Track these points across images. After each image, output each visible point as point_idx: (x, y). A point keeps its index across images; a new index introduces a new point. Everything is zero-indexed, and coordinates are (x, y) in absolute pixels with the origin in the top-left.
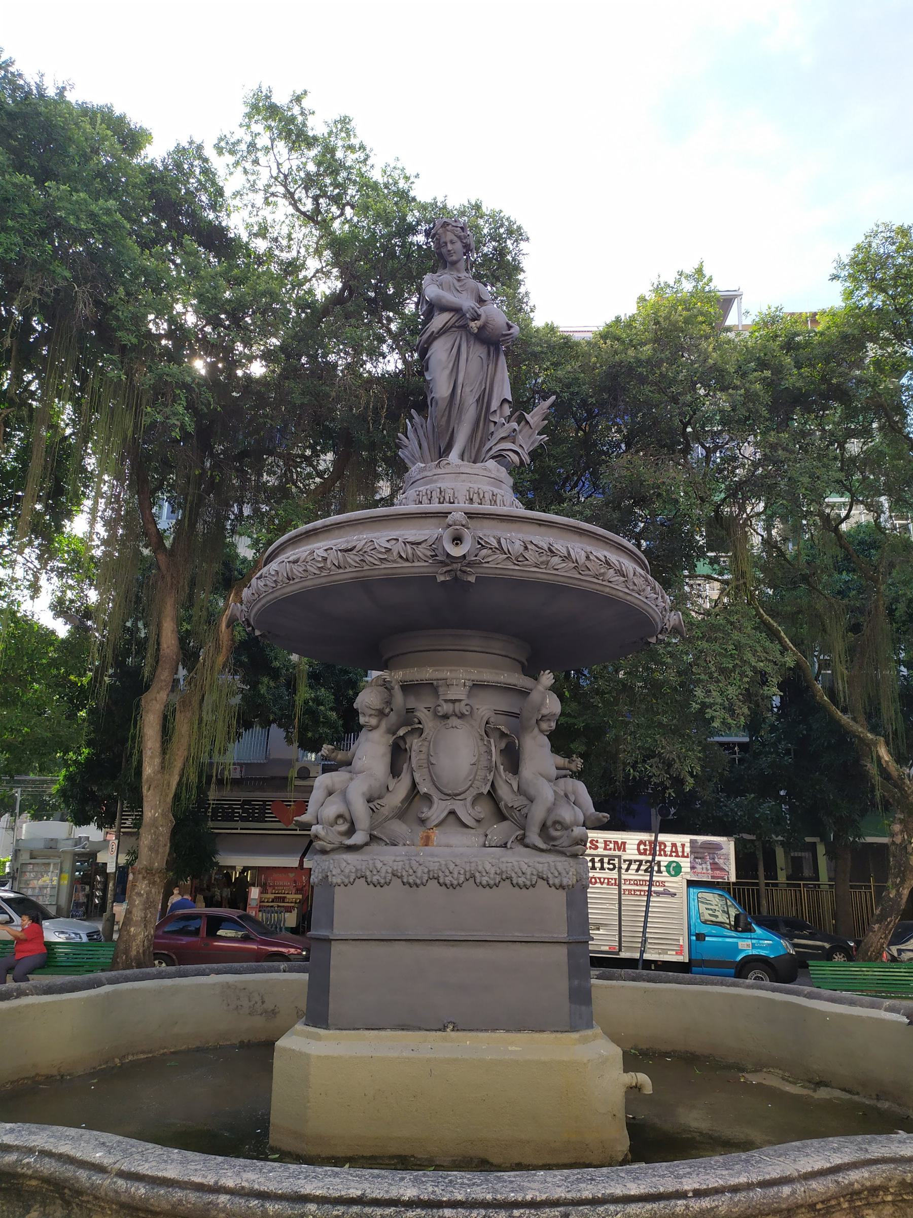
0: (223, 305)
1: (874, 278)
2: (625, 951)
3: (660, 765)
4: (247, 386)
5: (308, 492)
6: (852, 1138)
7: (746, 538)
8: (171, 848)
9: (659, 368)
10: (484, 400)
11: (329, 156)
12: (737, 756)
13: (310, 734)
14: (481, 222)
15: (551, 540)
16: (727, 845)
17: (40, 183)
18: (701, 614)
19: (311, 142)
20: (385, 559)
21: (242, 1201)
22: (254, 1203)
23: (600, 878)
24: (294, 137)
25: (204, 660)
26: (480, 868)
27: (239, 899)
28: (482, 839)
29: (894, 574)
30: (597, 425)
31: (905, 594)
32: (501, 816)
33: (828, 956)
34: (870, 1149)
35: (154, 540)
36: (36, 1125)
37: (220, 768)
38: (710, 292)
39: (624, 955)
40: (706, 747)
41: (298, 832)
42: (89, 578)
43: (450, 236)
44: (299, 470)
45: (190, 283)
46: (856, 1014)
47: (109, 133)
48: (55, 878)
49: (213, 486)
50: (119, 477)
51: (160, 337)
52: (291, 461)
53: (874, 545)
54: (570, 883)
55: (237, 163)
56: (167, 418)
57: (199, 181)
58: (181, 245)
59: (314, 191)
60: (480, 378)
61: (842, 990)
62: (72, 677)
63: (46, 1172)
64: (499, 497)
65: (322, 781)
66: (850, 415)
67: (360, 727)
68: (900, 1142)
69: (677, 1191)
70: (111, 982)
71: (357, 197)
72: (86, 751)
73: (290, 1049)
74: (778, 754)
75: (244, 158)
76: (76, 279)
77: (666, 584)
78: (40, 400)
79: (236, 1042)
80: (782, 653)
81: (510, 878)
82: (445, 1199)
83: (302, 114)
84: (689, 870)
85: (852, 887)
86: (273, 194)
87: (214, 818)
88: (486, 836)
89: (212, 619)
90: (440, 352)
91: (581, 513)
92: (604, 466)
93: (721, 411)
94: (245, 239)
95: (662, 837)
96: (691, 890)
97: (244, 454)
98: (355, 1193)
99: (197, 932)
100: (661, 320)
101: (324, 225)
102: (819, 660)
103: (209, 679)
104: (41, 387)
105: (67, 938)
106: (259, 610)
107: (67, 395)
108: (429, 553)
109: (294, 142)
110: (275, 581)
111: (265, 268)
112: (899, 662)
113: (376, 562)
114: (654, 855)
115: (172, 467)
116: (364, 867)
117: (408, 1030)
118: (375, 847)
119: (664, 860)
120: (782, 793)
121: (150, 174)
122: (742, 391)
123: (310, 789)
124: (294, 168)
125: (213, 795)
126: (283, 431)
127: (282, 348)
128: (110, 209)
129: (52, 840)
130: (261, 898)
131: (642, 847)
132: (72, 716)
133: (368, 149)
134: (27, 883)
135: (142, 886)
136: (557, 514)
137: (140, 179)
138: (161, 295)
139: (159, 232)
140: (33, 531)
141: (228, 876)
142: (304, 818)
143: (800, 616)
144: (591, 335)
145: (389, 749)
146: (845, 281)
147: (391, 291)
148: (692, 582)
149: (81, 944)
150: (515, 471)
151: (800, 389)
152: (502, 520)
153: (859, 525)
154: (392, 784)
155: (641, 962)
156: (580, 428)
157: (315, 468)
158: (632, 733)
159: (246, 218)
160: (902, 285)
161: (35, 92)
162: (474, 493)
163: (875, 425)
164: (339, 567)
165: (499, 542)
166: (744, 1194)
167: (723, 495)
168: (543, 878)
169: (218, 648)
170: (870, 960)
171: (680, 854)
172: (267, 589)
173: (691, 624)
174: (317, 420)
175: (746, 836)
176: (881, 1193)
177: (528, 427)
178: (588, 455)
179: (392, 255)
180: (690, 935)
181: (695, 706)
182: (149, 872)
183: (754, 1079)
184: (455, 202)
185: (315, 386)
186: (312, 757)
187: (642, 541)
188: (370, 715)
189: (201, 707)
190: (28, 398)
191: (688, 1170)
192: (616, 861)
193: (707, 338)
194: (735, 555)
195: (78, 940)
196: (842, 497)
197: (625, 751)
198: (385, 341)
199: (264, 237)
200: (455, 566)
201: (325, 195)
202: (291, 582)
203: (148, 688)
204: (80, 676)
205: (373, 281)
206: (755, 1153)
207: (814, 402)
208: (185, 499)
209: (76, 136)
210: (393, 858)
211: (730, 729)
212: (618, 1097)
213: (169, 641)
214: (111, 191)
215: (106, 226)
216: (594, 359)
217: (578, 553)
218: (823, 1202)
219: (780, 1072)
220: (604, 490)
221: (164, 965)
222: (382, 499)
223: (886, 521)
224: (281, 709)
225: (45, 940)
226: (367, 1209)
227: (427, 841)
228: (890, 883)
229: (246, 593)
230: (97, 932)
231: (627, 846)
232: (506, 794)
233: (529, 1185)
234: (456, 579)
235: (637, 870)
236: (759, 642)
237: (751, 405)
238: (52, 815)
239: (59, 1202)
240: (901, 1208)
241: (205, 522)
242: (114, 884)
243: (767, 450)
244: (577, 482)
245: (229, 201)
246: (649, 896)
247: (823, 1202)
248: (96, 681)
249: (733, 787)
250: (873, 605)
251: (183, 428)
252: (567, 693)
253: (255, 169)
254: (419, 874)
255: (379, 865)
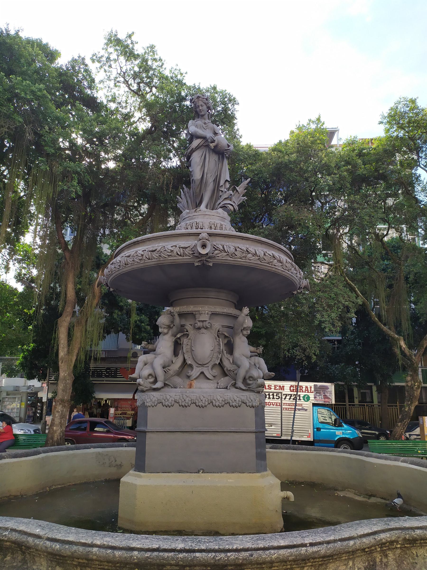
0: (95, 134)
1: (399, 123)
2: (284, 436)
3: (300, 350)
4: (107, 173)
5: (136, 223)
6: (382, 519)
7: (340, 244)
8: (73, 390)
9: (300, 165)
10: (217, 181)
11: (145, 63)
12: (336, 346)
13: (137, 337)
14: (216, 95)
15: (248, 246)
16: (331, 387)
17: (7, 75)
18: (319, 280)
19: (136, 57)
20: (170, 255)
21: (104, 550)
22: (109, 551)
23: (272, 403)
24: (128, 54)
25: (88, 302)
26: (215, 398)
27: (105, 414)
28: (216, 385)
30: (271, 192)
31: (413, 271)
32: (225, 374)
33: (377, 438)
34: (390, 524)
35: (63, 246)
36: (9, 517)
37: (96, 352)
38: (323, 129)
39: (283, 438)
40: (321, 342)
41: (132, 382)
42: (33, 264)
43: (200, 103)
44: (131, 212)
45: (79, 124)
46: (387, 464)
47: (40, 52)
48: (18, 405)
49: (91, 220)
50: (46, 216)
51: (65, 149)
52: (128, 208)
53: (399, 248)
54: (257, 405)
55: (101, 67)
56: (69, 188)
57: (83, 75)
58: (75, 106)
59: (138, 80)
60: (215, 170)
61: (383, 453)
62: (25, 310)
63: (14, 539)
64: (224, 226)
65: (142, 358)
66: (388, 187)
67: (160, 333)
68: (404, 520)
69: (302, 543)
70: (44, 452)
71: (158, 83)
72: (32, 345)
73: (127, 482)
74: (355, 345)
75: (104, 64)
76: (25, 122)
77: (302, 266)
78: (8, 179)
79: (103, 479)
80: (356, 298)
81: (229, 403)
82: (196, 549)
83: (132, 43)
84: (313, 398)
85: (389, 406)
86: (118, 82)
87: (93, 376)
88: (218, 383)
89: (91, 283)
90: (196, 157)
91: (263, 233)
92: (274, 211)
93: (329, 185)
94: (105, 102)
95: (301, 384)
96: (314, 408)
97: (105, 205)
98: (155, 546)
99: (85, 429)
100: (300, 142)
101: (143, 96)
102: (374, 301)
103: (90, 311)
104: (9, 173)
105: (24, 432)
106: (112, 278)
107: (21, 177)
108: (191, 252)
109: (128, 57)
110: (119, 265)
111: (115, 117)
112: (411, 302)
113: (166, 257)
114: (297, 392)
116: (178, 398)
117: (182, 473)
118: (166, 389)
119: (302, 394)
120: (357, 363)
121: (60, 72)
122: (338, 176)
123: (136, 362)
124: (128, 69)
125: (92, 365)
126: (124, 194)
127: (123, 155)
128: (41, 89)
129: (17, 386)
130: (115, 413)
131: (292, 388)
132: (25, 328)
133: (163, 60)
134: (5, 406)
135: (59, 408)
136: (252, 234)
137: (55, 74)
138: (65, 129)
139: (65, 99)
140: (6, 241)
141: (100, 403)
142: (134, 376)
143: (365, 281)
144: (267, 149)
145: (173, 343)
146: (386, 124)
147: (174, 128)
148: (315, 265)
149: (31, 435)
150: (232, 214)
151: (365, 175)
152: (225, 237)
153: (393, 238)
154: (174, 360)
155: (291, 441)
156: (263, 193)
157: (139, 212)
158: (287, 336)
159: (106, 93)
160: (412, 126)
161: (5, 32)
162: (212, 224)
163: (400, 192)
164: (149, 259)
165: (223, 247)
166: (332, 544)
167: (329, 225)
168: (244, 403)
169: (94, 296)
170: (396, 439)
171: (309, 391)
172: (115, 269)
173: (314, 284)
174: (140, 189)
175: (340, 383)
176: (395, 544)
177: (237, 193)
178: (266, 205)
180: (314, 428)
181: (317, 322)
182: (62, 401)
183: (342, 494)
184: (204, 85)
185: (139, 173)
186: (139, 347)
187: (292, 246)
188: (164, 328)
189: (86, 324)
190: (3, 179)
191: (308, 534)
192: (280, 395)
193: (322, 150)
194: (335, 252)
195: (29, 433)
196: (384, 225)
197: (284, 344)
198: (172, 152)
199: (114, 102)
200: (203, 258)
201: (143, 82)
202: (127, 266)
203: (61, 315)
204: (29, 310)
205: (166, 123)
206: (338, 527)
207: (372, 181)
208: (78, 226)
210: (175, 394)
211: (332, 333)
212: (278, 503)
213: (71, 294)
214: (41, 80)
215: (39, 97)
216: (269, 161)
217: (260, 252)
218: (368, 548)
219: (354, 491)
220: (274, 222)
221: (70, 444)
222: (171, 226)
223: (405, 236)
224: (124, 325)
225: (14, 433)
226: (161, 553)
227: (190, 386)
228: (405, 404)
229: (106, 271)
230: (38, 429)
231: (285, 388)
232: (227, 364)
233: (235, 542)
234: (203, 264)
235: (290, 399)
236: (346, 293)
237: (342, 182)
238: (17, 375)
239: (20, 552)
240: (404, 551)
241: (88, 237)
242: (46, 407)
243: (350, 204)
244: (262, 218)
245: (98, 85)
246: (295, 410)
247: (368, 548)
248: (37, 312)
249: (334, 360)
250: (398, 276)
251: (76, 193)
252: (257, 317)
253: (110, 70)
254: (187, 401)
255: (168, 397)
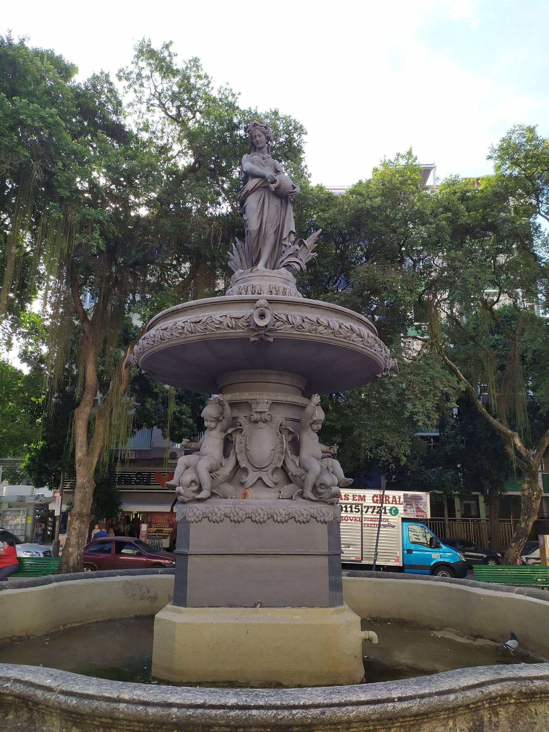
0: (122, 172)
1: (513, 158)
2: (365, 560)
3: (386, 450)
4: (138, 222)
5: (175, 286)
6: (491, 666)
7: (437, 314)
8: (93, 500)
9: (385, 211)
10: (279, 232)
11: (186, 81)
12: (432, 444)
13: (177, 433)
14: (278, 122)
15: (319, 316)
16: (426, 497)
17: (10, 97)
18: (410, 359)
19: (175, 73)
20: (219, 328)
21: (133, 707)
22: (140, 708)
23: (350, 517)
24: (165, 70)
25: (113, 388)
26: (276, 512)
27: (135, 531)
28: (278, 494)
29: (525, 336)
30: (348, 246)
31: (531, 348)
32: (289, 481)
33: (485, 562)
34: (502, 673)
35: (82, 315)
36: (11, 665)
37: (123, 453)
38: (416, 165)
39: (364, 562)
40: (413, 439)
41: (170, 491)
42: (43, 339)
43: (258, 132)
44: (169, 273)
45: (102, 159)
46: (498, 595)
47: (51, 66)
48: (24, 519)
49: (117, 283)
50: (60, 277)
51: (84, 192)
52: (164, 268)
53: (513, 318)
54: (330, 520)
55: (130, 86)
56: (89, 241)
57: (107, 97)
58: (96, 136)
59: (177, 103)
60: (277, 218)
61: (492, 582)
62: (33, 399)
63: (18, 692)
64: (288, 290)
65: (182, 460)
66: (499, 240)
67: (206, 428)
68: (519, 668)
69: (388, 698)
70: (57, 580)
71: (203, 107)
72: (41, 443)
73: (164, 619)
74: (456, 443)
75: (134, 83)
76: (32, 156)
77: (388, 342)
78: (11, 230)
79: (132, 615)
80: (458, 383)
81: (294, 517)
82: (252, 704)
83: (170, 55)
84: (403, 512)
85: (500, 521)
86: (152, 105)
87: (119, 483)
88: (280, 492)
89: (117, 363)
90: (252, 202)
91: (338, 299)
92: (353, 271)
93: (422, 238)
94: (135, 131)
95: (387, 493)
96: (404, 523)
97: (135, 264)
98: (200, 701)
99: (109, 551)
100: (386, 183)
101: (183, 124)
102: (480, 386)
103: (115, 399)
104: (11, 222)
105: (31, 555)
106: (144, 358)
107: (27, 227)
108: (245, 324)
109: (165, 73)
110: (153, 341)
111: (147, 150)
112: (528, 388)
113: (214, 330)
114: (382, 503)
115: (92, 271)
116: (229, 511)
117: (234, 607)
118: (213, 500)
119: (388, 506)
120: (459, 466)
121: (77, 92)
122: (434, 226)
123: (175, 465)
124: (165, 89)
125: (118, 469)
126: (159, 249)
127: (158, 199)
129: (22, 496)
130: (148, 530)
131: (375, 498)
132: (33, 422)
133: (210, 77)
134: (7, 522)
135: (76, 524)
136: (324, 300)
137: (71, 95)
138: (84, 166)
139: (83, 127)
140: (8, 310)
141: (128, 518)
142: (172, 482)
143: (469, 360)
144: (344, 191)
145: (223, 441)
146: (496, 160)
147: (224, 164)
148: (405, 340)
149: (40, 559)
150: (299, 275)
151: (469, 225)
152: (289, 304)
153: (505, 306)
154: (224, 462)
155: (374, 567)
156: (338, 248)
157: (179, 272)
158: (369, 431)
159: (136, 119)
160: (529, 162)
161: (6, 41)
162: (273, 288)
163: (514, 246)
164: (192, 333)
165: (287, 318)
166: (427, 699)
167: (423, 288)
168: (313, 517)
169: (121, 381)
170: (510, 564)
171: (398, 502)
172: (148, 346)
173: (404, 365)
174: (180, 243)
175: (437, 492)
176: (508, 698)
177: (305, 248)
178: (343, 264)
179: (225, 142)
180: (403, 550)
181: (407, 414)
182: (80, 515)
183: (439, 634)
184: (263, 109)
185: (178, 222)
186: (178, 446)
187: (376, 316)
188: (211, 421)
189: (111, 417)
190: (4, 229)
191: (396, 686)
192: (360, 507)
193: (413, 193)
194: (430, 324)
195: (38, 556)
196: (494, 289)
197: (365, 441)
198: (221, 195)
199: (147, 131)
200: (261, 332)
201: (183, 105)
202: (163, 342)
203: (78, 404)
204: (37, 397)
205: (213, 158)
206: (434, 676)
207: (478, 232)
208: (100, 291)
209: (31, 69)
210: (225, 506)
212: (357, 646)
213: (91, 377)
214: (53, 103)
215: (51, 124)
217: (334, 324)
218: (473, 704)
219: (455, 630)
220: (352, 285)
221: (90, 570)
222: (219, 291)
223: (520, 304)
224: (159, 417)
225: (18, 556)
226: (207, 711)
227: (245, 496)
228: (521, 519)
229: (136, 348)
230: (49, 552)
231: (366, 498)
232: (292, 468)
233: (302, 696)
234: (261, 339)
235: (372, 512)
236: (444, 376)
237: (440, 234)
238: (21, 482)
239: (25, 709)
240: (520, 707)
241: (113, 305)
242: (59, 523)
243: (449, 262)
244: (337, 280)
245: (126, 109)
246: (379, 527)
247: (473, 704)
248: (47, 401)
249: (429, 463)
250: (512, 354)
251: (98, 248)
252: (330, 407)
253: (141, 89)
254: (240, 515)
255: (216, 510)
